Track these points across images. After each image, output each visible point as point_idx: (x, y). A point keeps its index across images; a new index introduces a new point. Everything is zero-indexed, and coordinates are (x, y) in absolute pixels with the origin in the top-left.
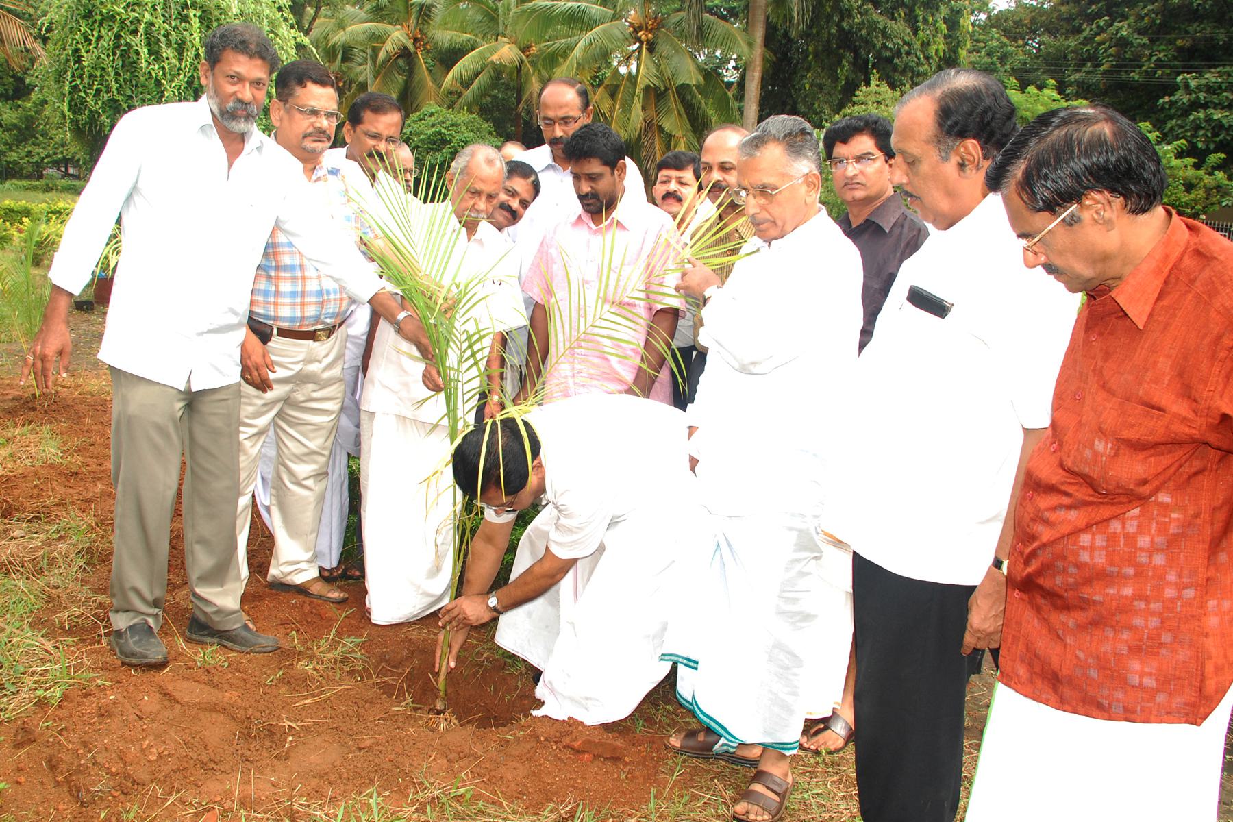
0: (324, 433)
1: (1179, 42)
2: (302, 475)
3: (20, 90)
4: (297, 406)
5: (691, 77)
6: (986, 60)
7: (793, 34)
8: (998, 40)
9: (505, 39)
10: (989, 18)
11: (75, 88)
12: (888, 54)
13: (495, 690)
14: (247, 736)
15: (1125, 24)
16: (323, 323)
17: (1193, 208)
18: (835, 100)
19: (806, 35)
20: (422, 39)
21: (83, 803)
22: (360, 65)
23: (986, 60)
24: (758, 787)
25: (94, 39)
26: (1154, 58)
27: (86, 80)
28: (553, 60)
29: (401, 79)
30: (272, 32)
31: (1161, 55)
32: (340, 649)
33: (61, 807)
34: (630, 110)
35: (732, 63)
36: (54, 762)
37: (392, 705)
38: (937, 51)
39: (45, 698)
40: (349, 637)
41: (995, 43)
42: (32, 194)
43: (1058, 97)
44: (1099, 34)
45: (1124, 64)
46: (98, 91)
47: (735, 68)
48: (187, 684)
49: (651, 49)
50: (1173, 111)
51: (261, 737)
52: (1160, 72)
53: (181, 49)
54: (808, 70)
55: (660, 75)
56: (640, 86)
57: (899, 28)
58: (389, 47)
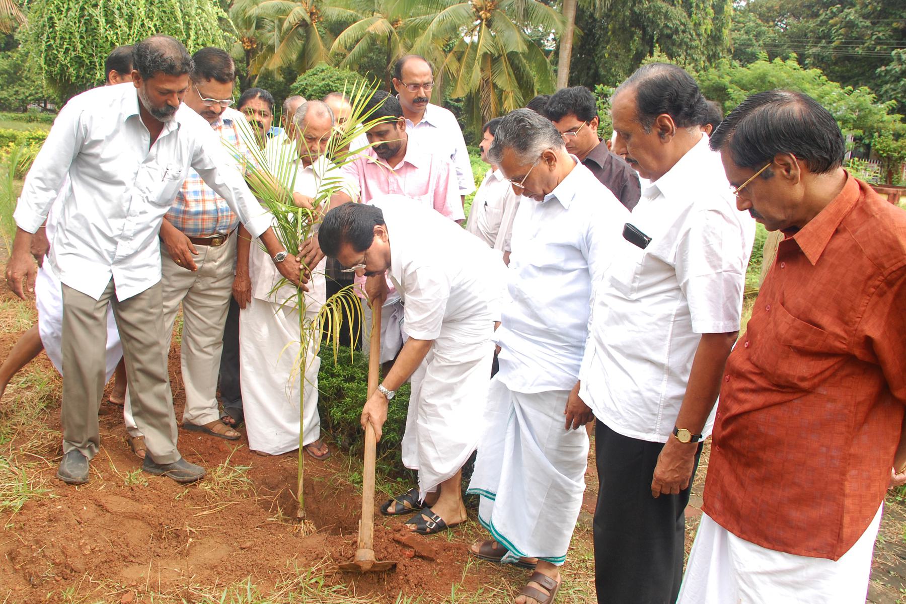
0: (220, 313)
1: (894, 25)
2: (203, 345)
3: (10, 44)
4: (199, 294)
5: (518, 46)
6: (745, 37)
7: (597, 15)
8: (754, 21)
9: (379, 15)
10: (748, 4)
11: (50, 47)
12: (669, 32)
13: (346, 507)
14: (159, 538)
15: (853, 10)
16: (218, 233)
17: (899, 152)
18: (627, 66)
19: (607, 16)
20: (316, 13)
21: (33, 585)
22: (269, 32)
23: (745, 37)
24: (534, 585)
25: (64, 10)
26: (874, 37)
27: (58, 41)
28: (414, 31)
29: (300, 43)
30: (200, 8)
31: (880, 35)
32: (231, 474)
33: (17, 588)
34: (472, 71)
35: (552, 36)
36: (13, 555)
37: (268, 517)
38: (706, 29)
39: (10, 507)
40: (239, 465)
41: (752, 24)
42: (17, 123)
43: (798, 67)
44: (831, 18)
45: (850, 41)
46: (67, 50)
47: (554, 40)
48: (116, 498)
49: (489, 25)
50: (888, 78)
51: (170, 538)
52: (878, 48)
53: (130, 19)
54: (608, 42)
55: (495, 45)
56: (480, 53)
57: (678, 12)
58: (291, 19)
